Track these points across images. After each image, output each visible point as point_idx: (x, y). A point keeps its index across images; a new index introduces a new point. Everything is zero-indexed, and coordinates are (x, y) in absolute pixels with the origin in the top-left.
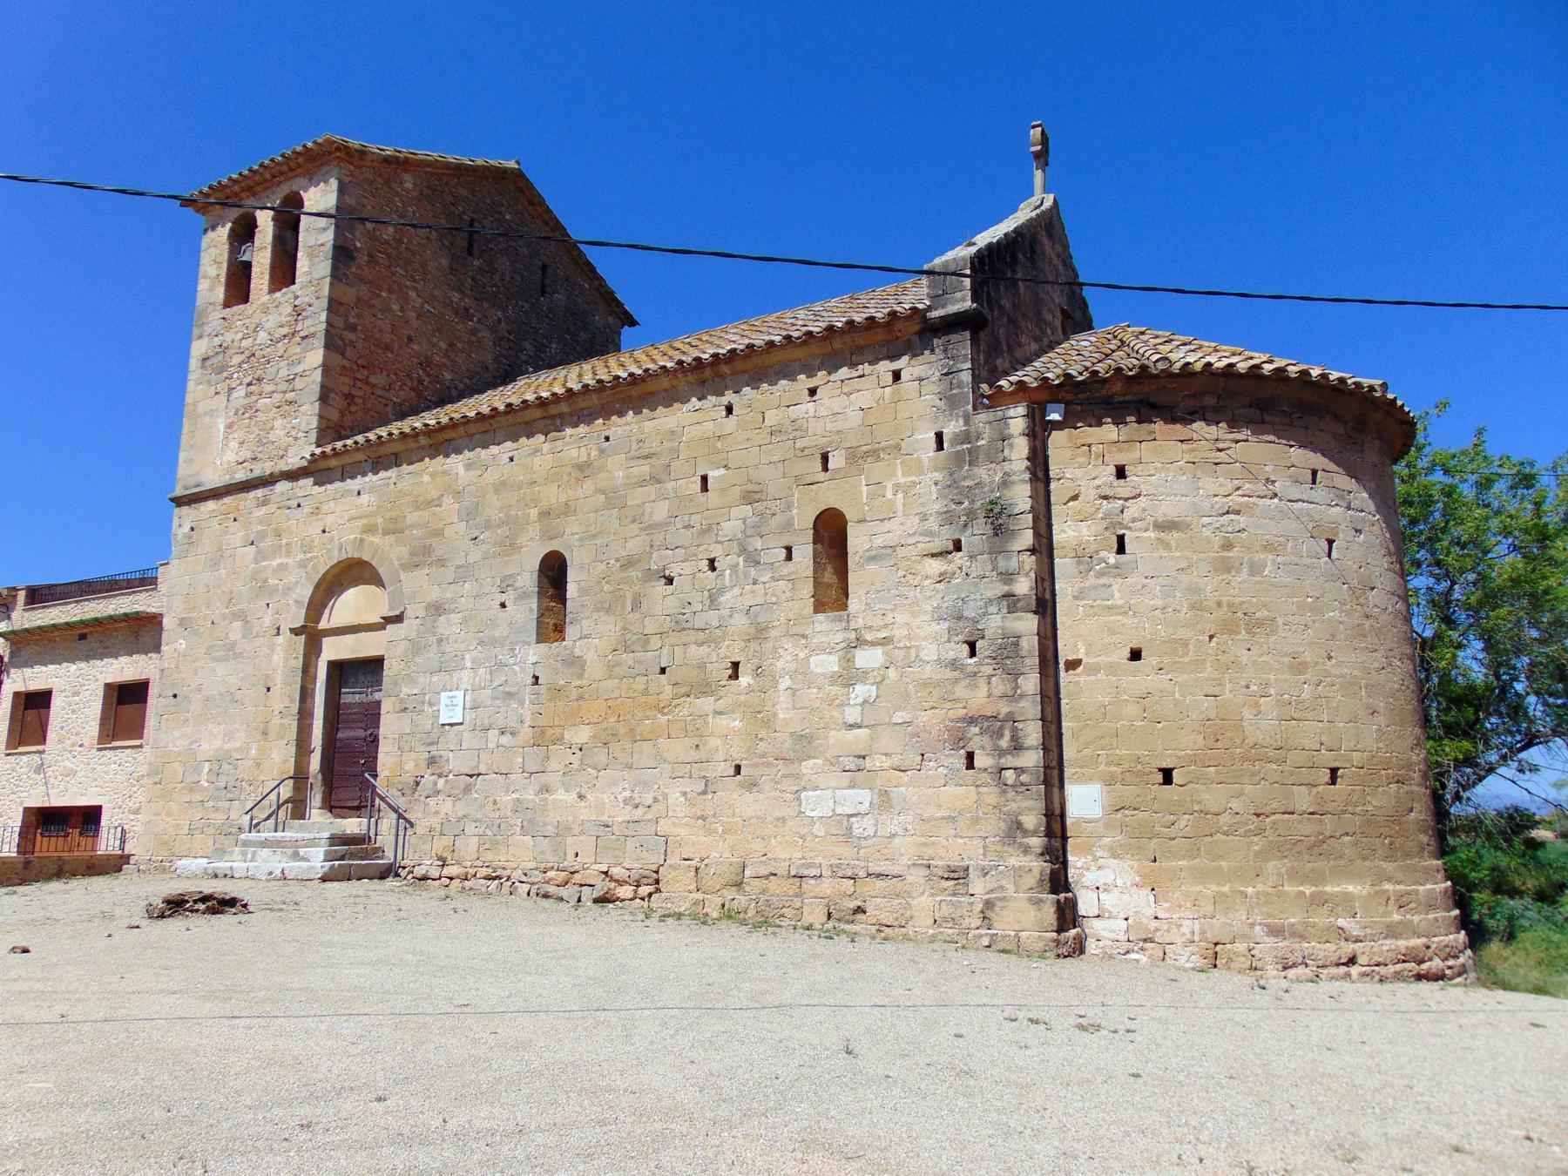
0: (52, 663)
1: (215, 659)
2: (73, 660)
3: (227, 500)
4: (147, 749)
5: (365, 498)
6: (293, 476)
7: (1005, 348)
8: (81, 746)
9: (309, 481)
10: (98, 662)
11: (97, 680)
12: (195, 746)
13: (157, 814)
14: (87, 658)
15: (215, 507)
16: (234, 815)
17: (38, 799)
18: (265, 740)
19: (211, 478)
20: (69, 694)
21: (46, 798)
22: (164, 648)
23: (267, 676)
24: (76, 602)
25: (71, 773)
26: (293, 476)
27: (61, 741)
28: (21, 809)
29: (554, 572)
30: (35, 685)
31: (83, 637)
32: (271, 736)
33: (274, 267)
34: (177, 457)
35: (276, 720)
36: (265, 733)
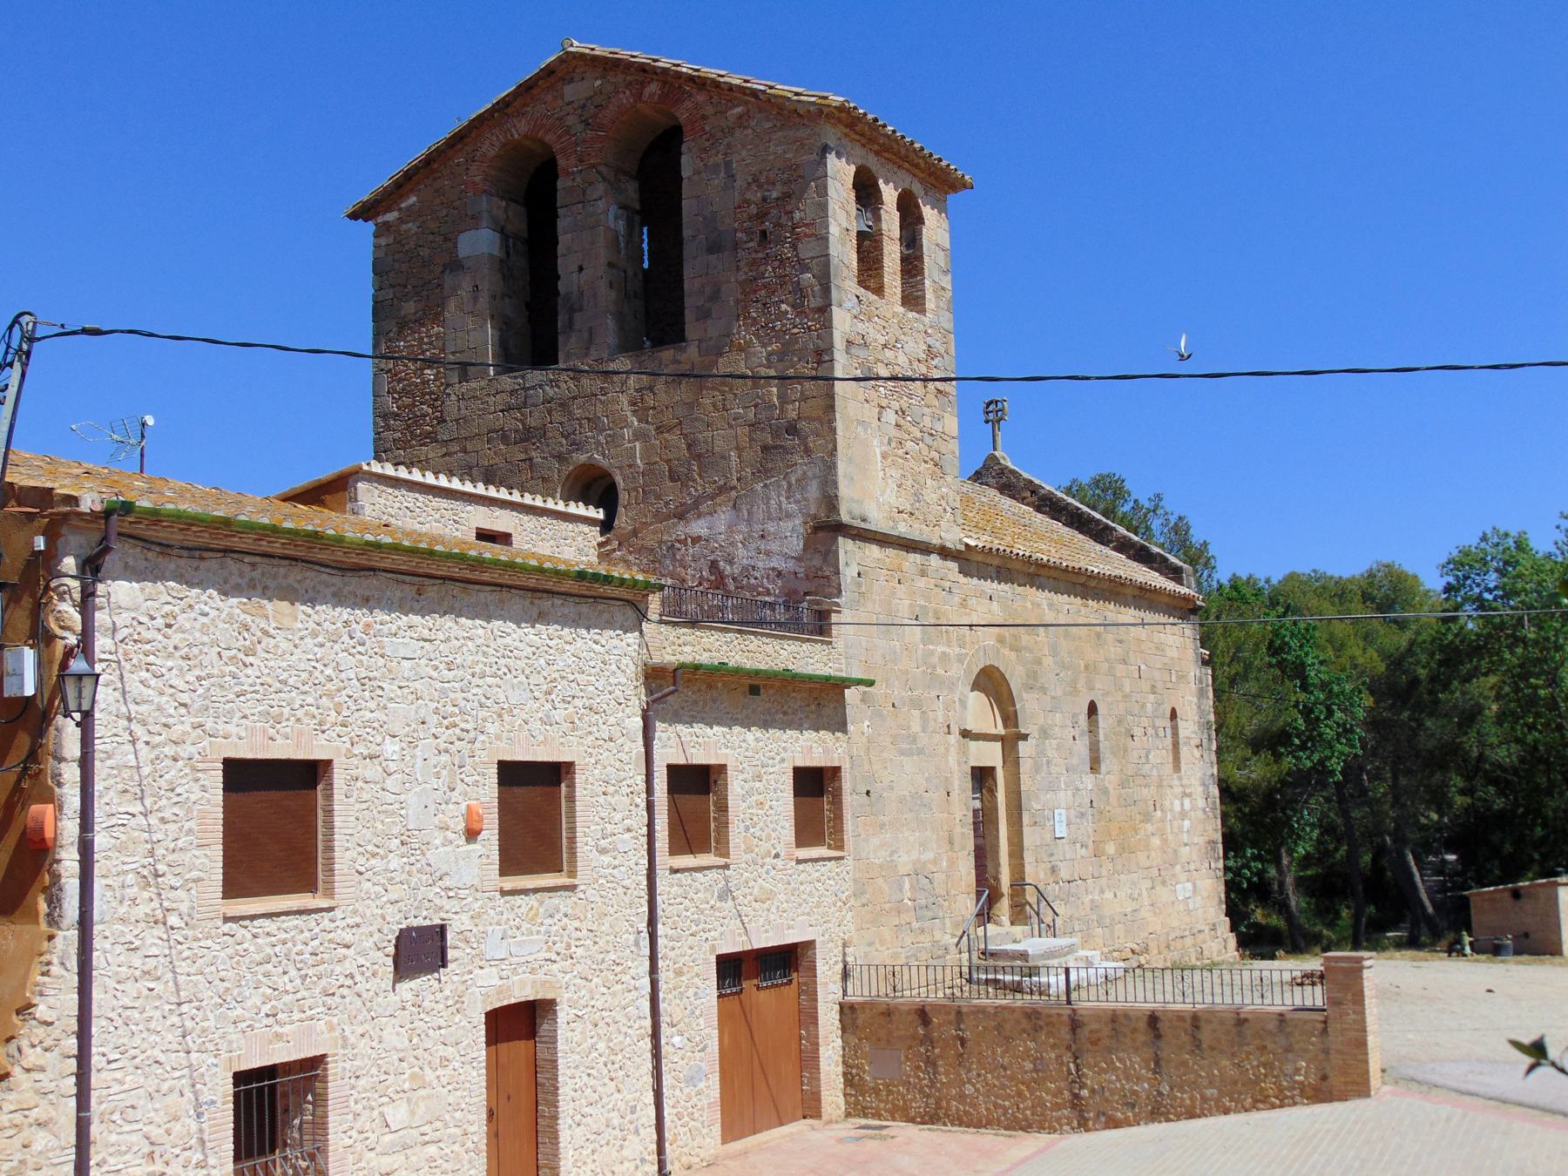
0: (718, 724)
1: (902, 753)
2: (747, 726)
3: (891, 552)
4: (849, 861)
5: (995, 606)
6: (944, 553)
7: (713, 844)
8: (777, 856)
9: (953, 566)
10: (778, 733)
11: (783, 760)
12: (895, 857)
13: (871, 944)
14: (765, 725)
15: (880, 556)
16: (938, 935)
17: (733, 945)
18: (952, 850)
19: (1178, 640)
20: (749, 777)
21: (744, 938)
22: (851, 728)
23: (946, 778)
24: (739, 632)
25: (767, 897)
26: (944, 553)
27: (749, 850)
28: (714, 959)
29: (1092, 709)
30: (699, 758)
31: (754, 690)
32: (957, 847)
33: (878, 247)
34: (556, 321)
35: (958, 829)
36: (951, 843)
